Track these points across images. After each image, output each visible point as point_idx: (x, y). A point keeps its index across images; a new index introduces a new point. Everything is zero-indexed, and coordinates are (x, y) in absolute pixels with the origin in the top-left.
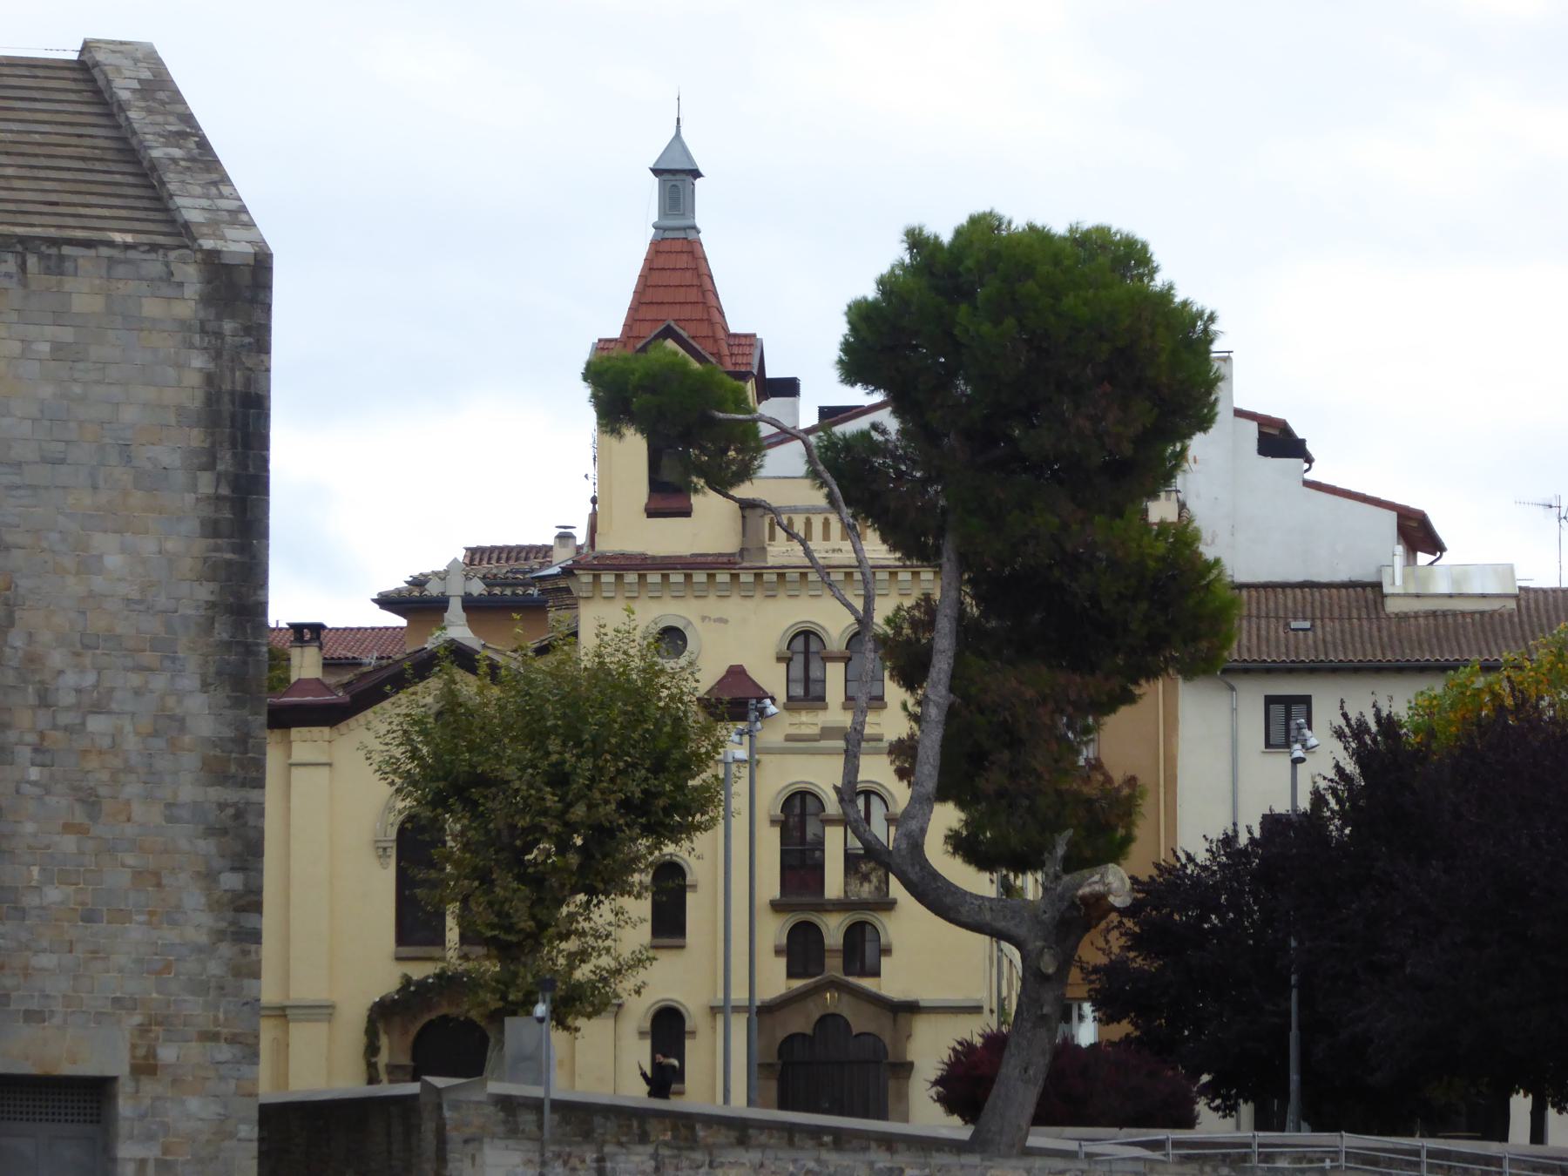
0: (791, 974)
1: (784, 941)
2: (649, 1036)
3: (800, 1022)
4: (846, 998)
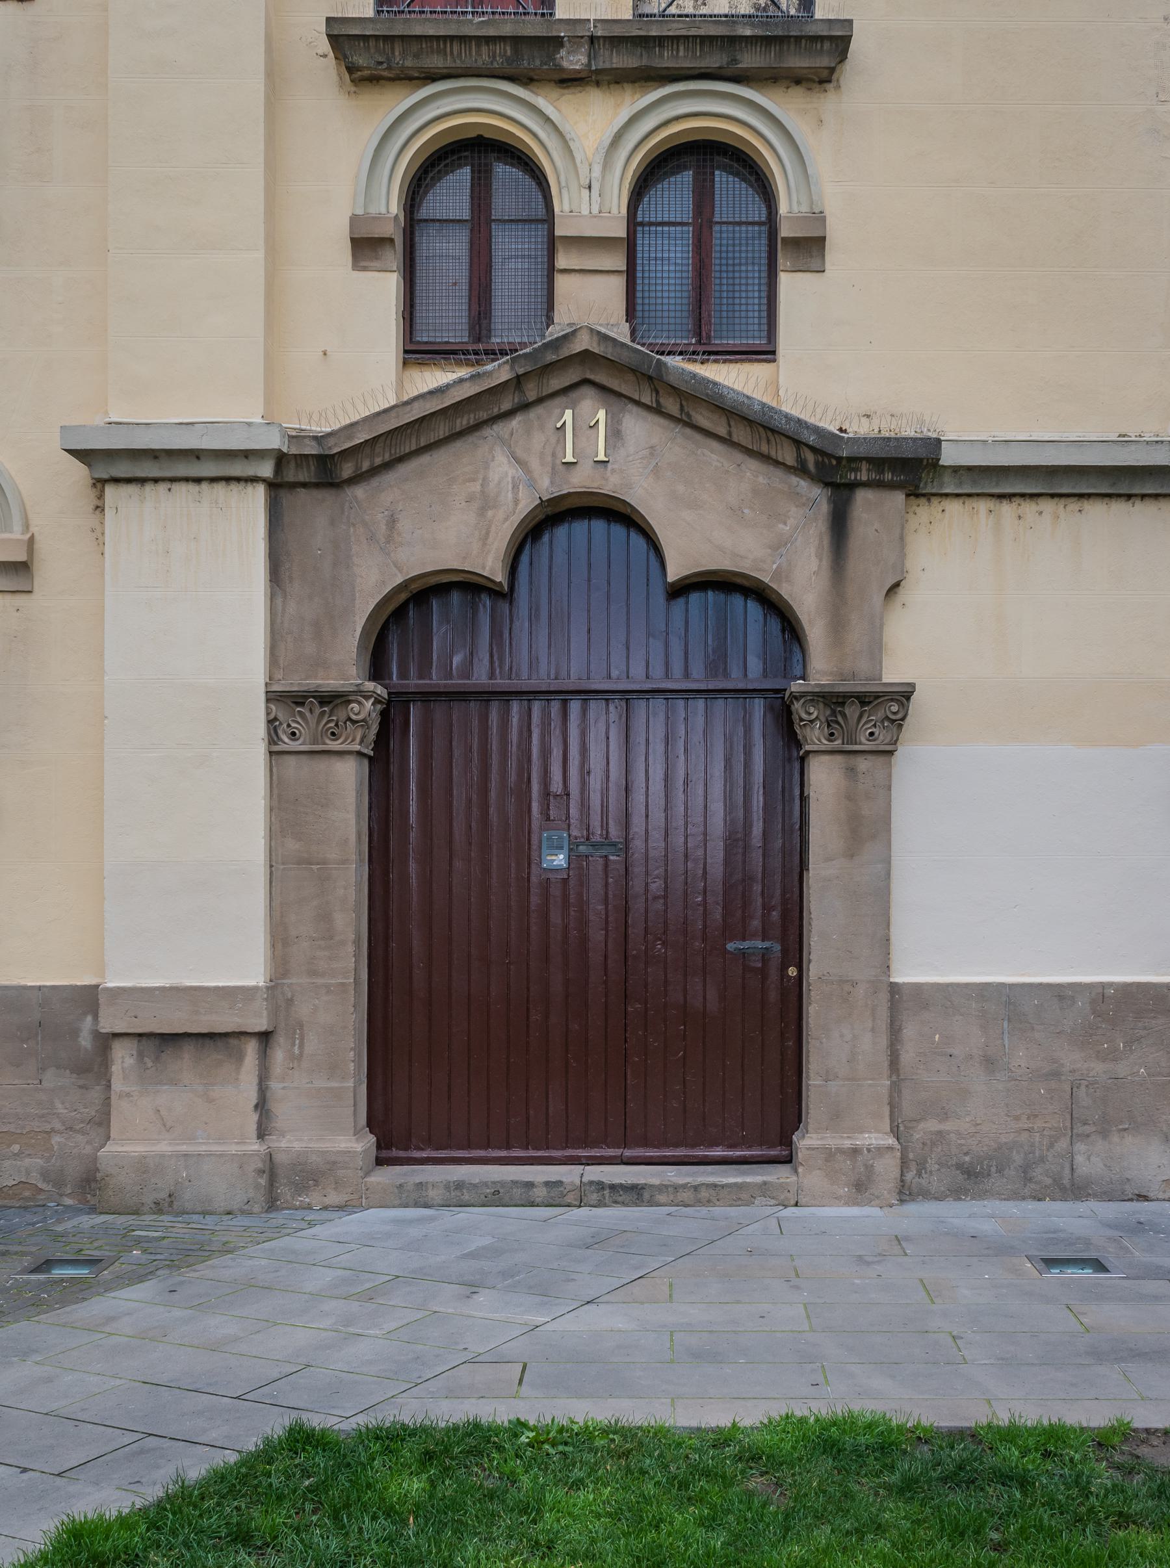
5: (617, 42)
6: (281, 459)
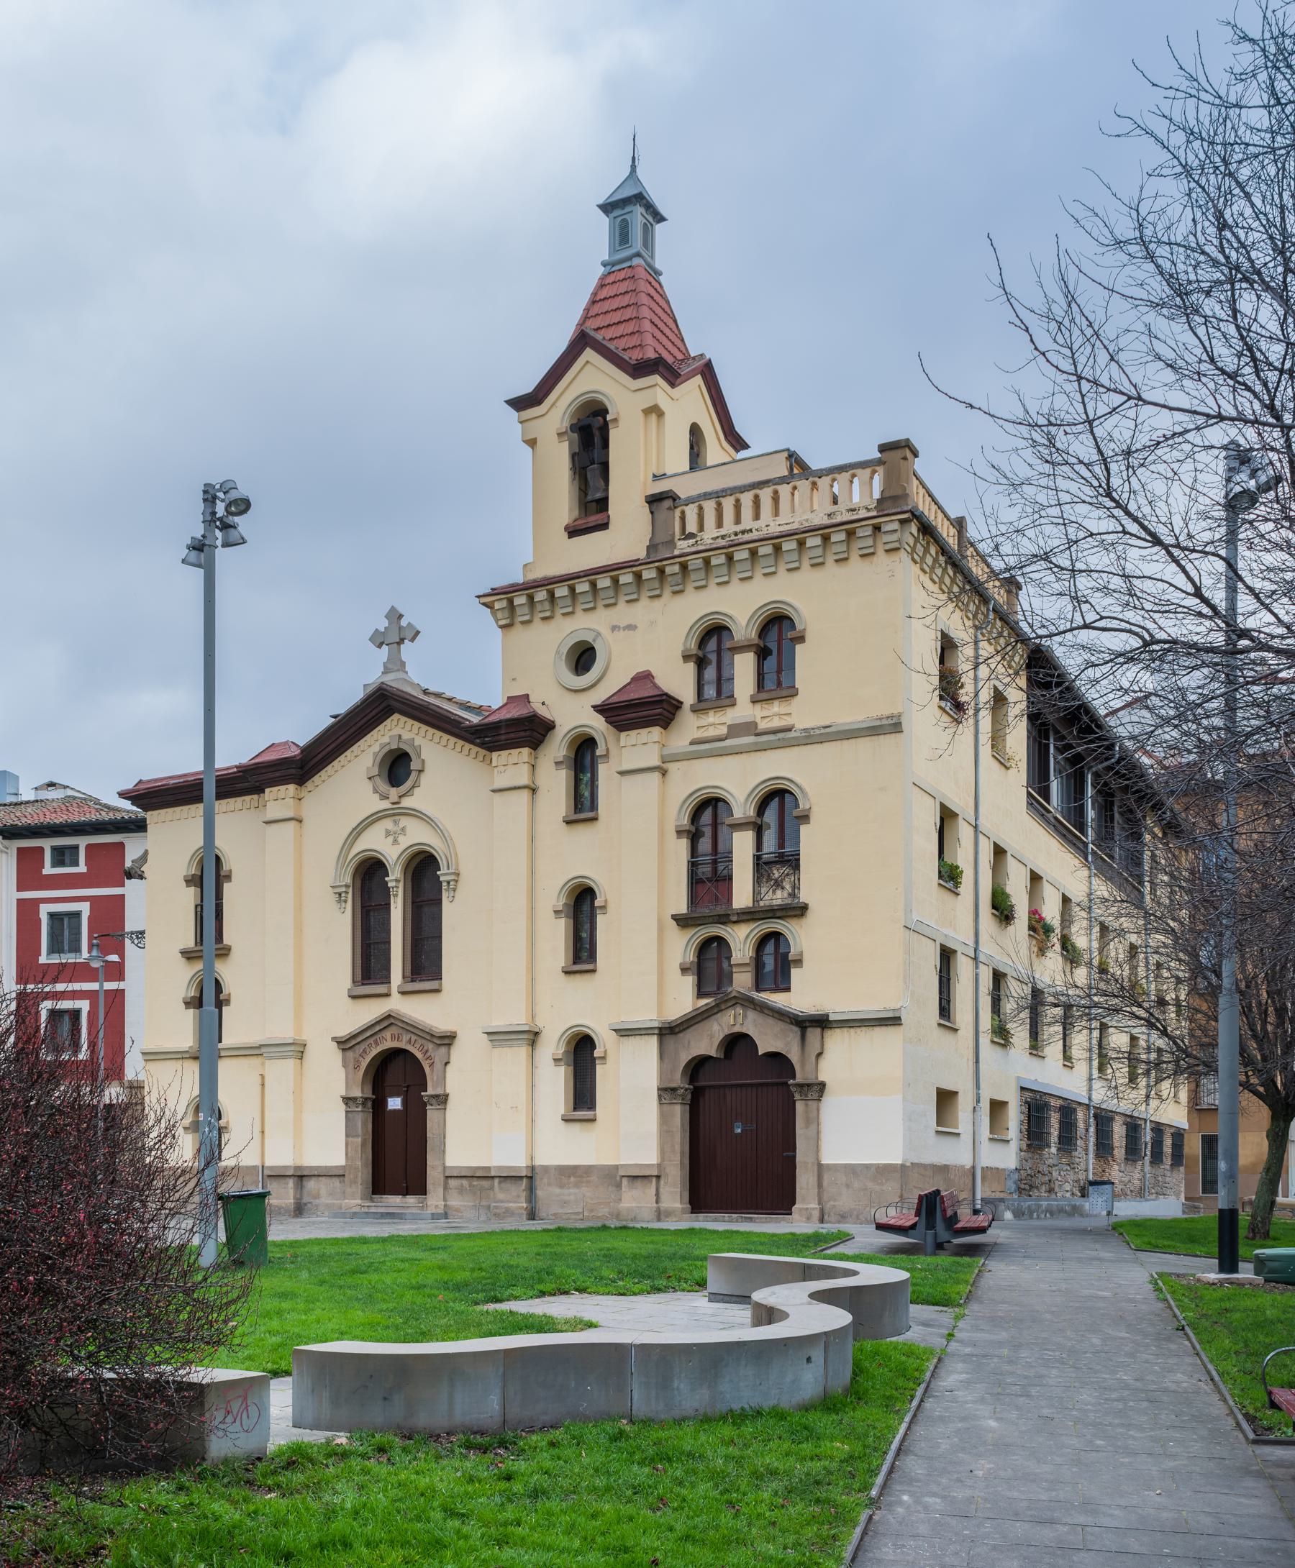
0: (700, 994)
3: (706, 1042)
4: (751, 1015)
5: (744, 913)
6: (660, 1029)
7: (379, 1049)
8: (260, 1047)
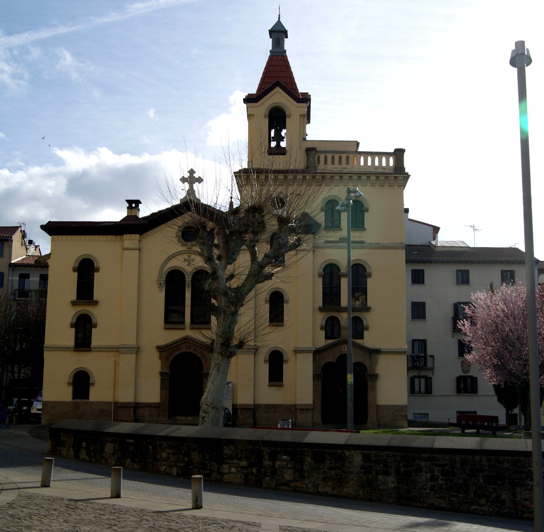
0: (327, 338)
1: (324, 324)
2: (268, 362)
3: (331, 357)
7: (179, 352)
8: (118, 348)
